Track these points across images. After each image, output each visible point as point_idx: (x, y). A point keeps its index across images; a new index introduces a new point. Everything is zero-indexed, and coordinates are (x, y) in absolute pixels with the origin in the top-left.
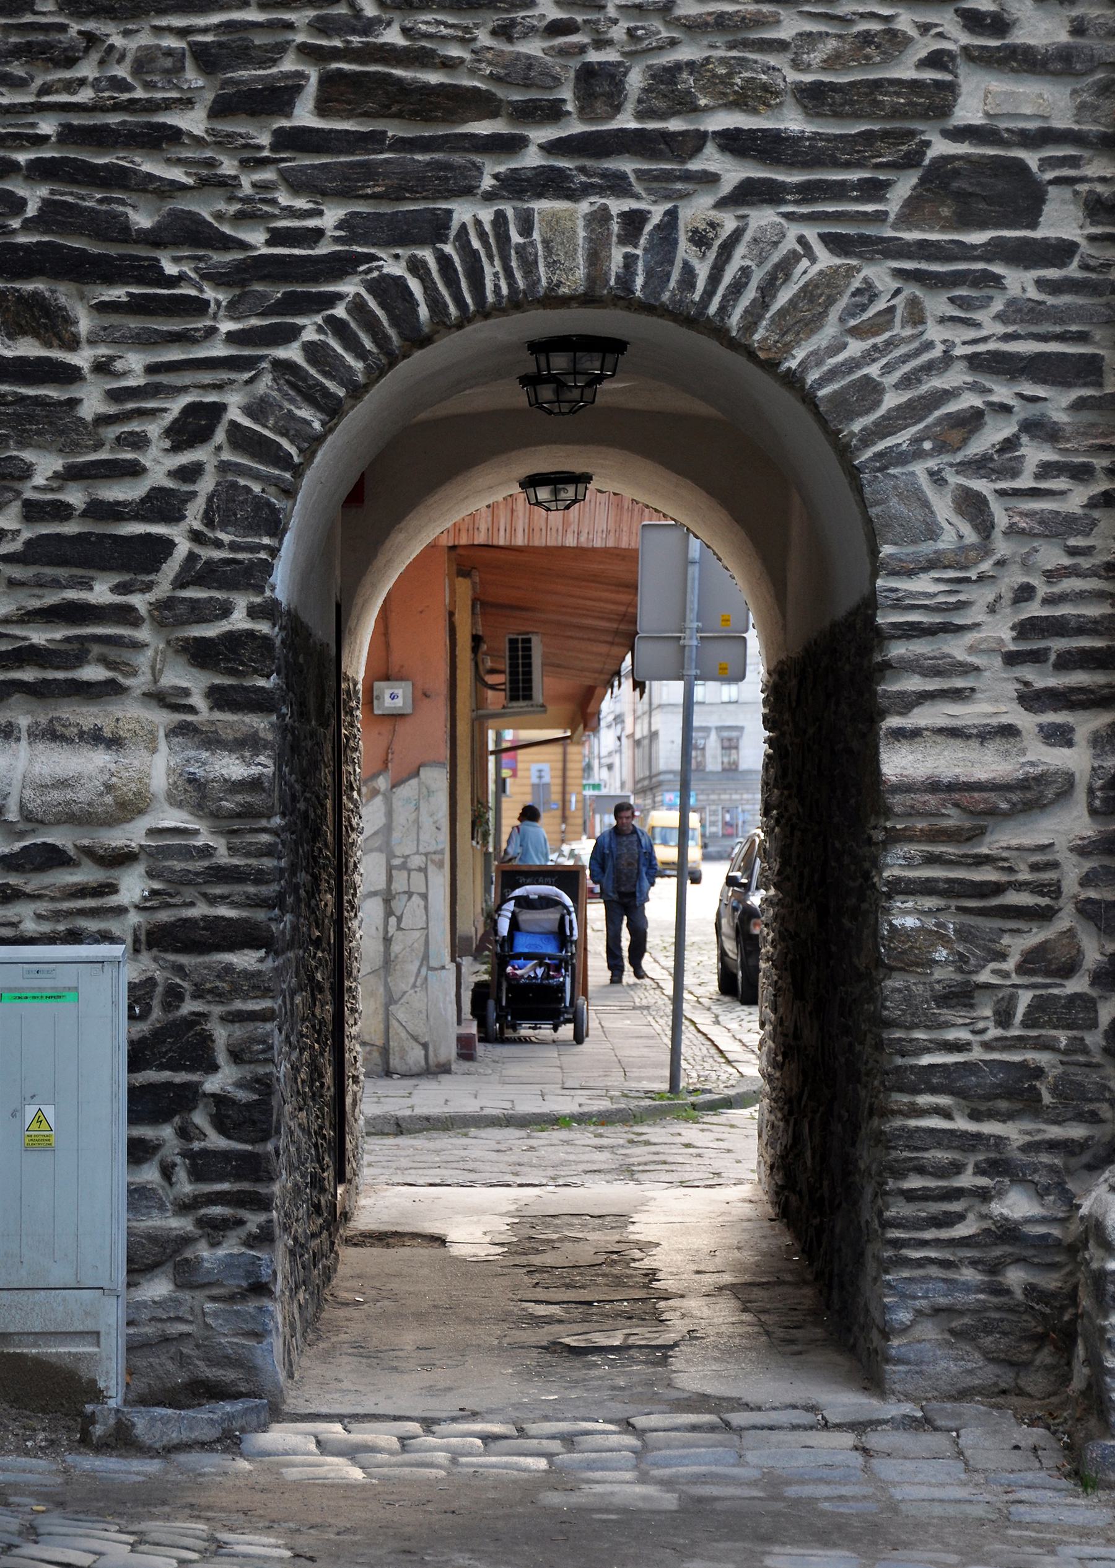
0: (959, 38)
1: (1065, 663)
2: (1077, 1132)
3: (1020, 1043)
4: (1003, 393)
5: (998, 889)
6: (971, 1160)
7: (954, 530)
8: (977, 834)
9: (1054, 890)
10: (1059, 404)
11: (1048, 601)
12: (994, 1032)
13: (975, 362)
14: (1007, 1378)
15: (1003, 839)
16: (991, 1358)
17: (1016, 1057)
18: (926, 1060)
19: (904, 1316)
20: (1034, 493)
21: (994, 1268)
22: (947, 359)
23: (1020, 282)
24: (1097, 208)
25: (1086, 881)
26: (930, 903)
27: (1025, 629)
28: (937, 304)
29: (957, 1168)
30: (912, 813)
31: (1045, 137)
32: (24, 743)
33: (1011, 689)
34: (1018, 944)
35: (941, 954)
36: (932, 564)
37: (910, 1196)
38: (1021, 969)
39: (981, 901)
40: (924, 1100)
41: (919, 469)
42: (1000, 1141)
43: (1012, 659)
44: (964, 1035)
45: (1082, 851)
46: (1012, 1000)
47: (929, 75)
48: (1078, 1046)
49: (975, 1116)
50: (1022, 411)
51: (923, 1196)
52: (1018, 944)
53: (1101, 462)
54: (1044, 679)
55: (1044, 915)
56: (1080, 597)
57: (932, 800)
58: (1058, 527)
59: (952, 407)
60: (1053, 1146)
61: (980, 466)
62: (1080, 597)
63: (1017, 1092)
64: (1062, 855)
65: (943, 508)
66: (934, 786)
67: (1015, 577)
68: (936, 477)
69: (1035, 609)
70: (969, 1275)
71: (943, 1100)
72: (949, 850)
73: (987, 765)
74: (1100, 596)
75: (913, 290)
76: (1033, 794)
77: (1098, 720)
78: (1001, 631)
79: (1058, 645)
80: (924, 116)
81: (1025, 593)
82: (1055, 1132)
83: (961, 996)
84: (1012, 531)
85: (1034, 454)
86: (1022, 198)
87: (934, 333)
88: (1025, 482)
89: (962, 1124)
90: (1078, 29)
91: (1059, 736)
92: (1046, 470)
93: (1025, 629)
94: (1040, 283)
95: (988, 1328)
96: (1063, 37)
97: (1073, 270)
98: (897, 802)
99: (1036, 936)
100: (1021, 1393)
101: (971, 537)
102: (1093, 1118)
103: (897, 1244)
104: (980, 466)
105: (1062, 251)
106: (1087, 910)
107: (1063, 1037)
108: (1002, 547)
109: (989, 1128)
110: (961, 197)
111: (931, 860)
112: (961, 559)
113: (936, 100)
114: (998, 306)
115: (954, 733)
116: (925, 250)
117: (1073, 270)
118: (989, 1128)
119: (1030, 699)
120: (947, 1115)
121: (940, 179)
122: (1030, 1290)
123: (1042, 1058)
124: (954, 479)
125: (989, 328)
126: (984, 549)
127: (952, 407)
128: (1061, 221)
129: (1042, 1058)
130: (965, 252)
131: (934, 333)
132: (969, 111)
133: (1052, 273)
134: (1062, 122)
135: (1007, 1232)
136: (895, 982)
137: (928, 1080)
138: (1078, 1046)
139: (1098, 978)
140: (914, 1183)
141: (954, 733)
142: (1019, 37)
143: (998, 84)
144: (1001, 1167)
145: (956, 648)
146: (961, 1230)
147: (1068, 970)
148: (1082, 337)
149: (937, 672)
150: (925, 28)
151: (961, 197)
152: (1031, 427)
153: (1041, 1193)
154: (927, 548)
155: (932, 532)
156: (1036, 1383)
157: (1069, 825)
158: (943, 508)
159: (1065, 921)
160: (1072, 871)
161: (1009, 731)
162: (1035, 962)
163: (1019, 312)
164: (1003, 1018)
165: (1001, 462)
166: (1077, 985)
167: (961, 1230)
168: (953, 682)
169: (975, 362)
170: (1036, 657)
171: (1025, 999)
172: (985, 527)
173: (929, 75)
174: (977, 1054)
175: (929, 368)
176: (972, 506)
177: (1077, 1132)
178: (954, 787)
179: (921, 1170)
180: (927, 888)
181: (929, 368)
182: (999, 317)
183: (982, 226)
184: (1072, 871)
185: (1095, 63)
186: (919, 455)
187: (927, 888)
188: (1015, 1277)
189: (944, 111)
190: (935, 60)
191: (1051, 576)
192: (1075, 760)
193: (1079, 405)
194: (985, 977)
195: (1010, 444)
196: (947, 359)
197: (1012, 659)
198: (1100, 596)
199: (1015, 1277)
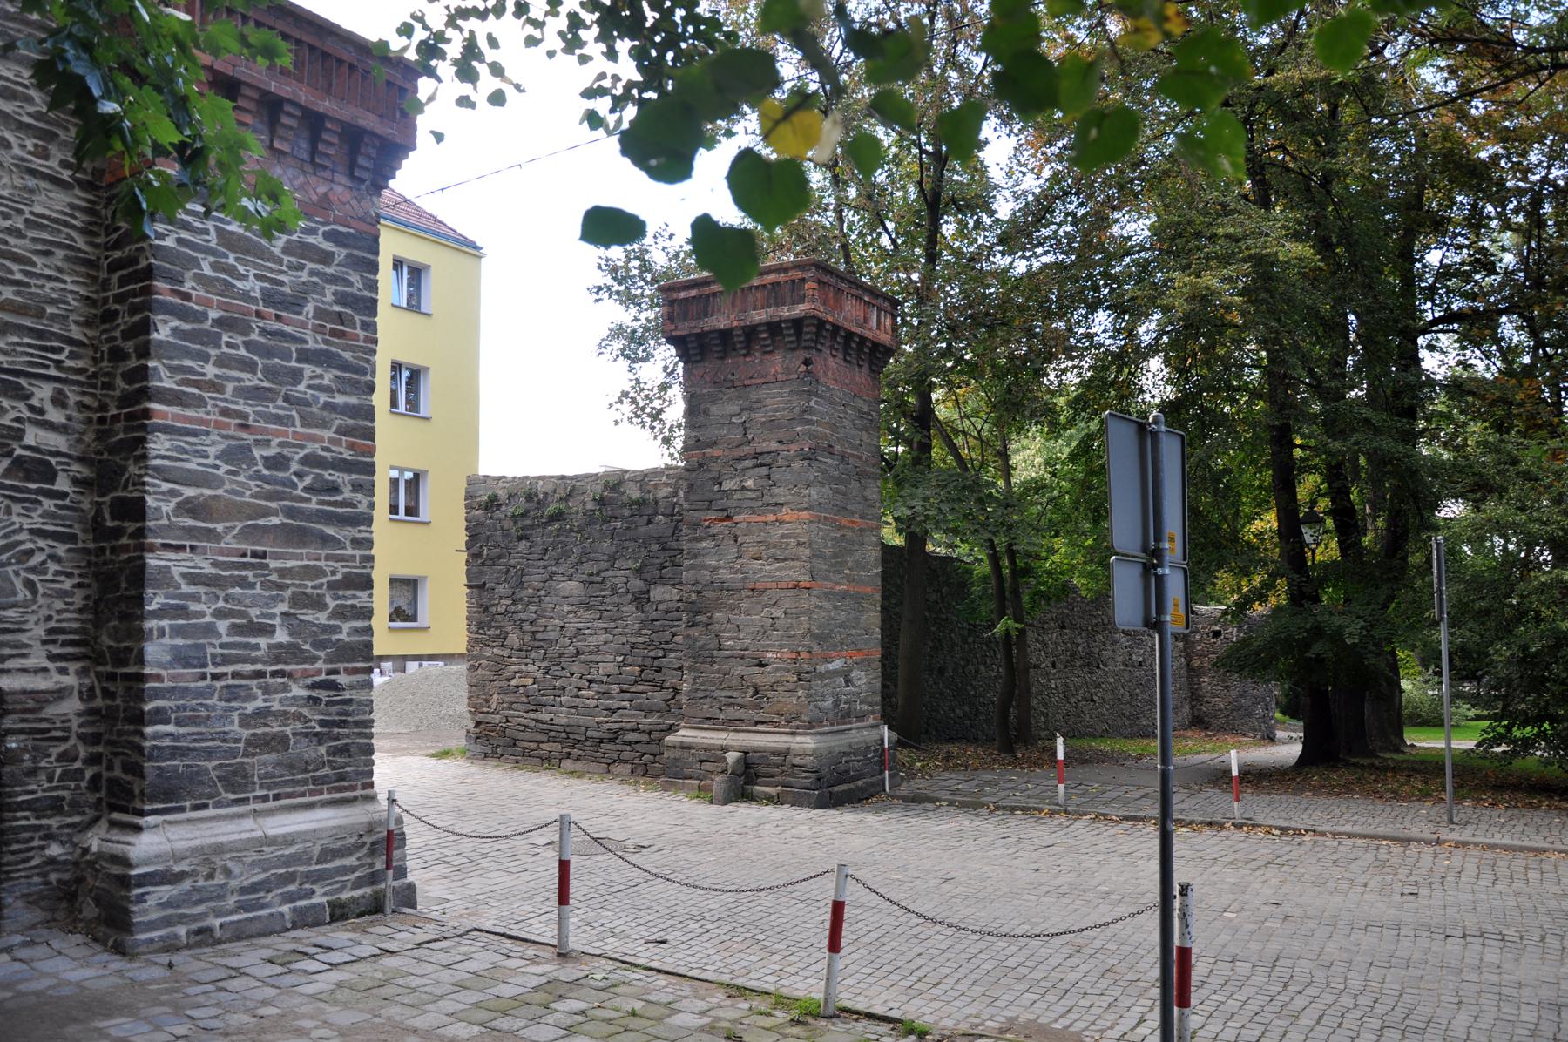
0: (26, 414)
1: (64, 644)
2: (77, 819)
3: (56, 788)
4: (41, 543)
5: (49, 730)
6: (37, 835)
7: (23, 594)
8: (41, 709)
9: (68, 730)
10: (61, 549)
11: (59, 621)
12: (46, 785)
13: (31, 531)
14: (49, 916)
15: (50, 711)
16: (43, 909)
17: (54, 794)
18: (20, 799)
19: (10, 900)
20: (53, 581)
21: (45, 875)
22: (21, 529)
23: (48, 504)
24: (75, 481)
25: (80, 726)
26: (22, 737)
27: (50, 631)
28: (17, 508)
29: (32, 839)
30: (15, 702)
31: (57, 454)
32: (410, 878)
33: (44, 654)
34: (55, 751)
35: (27, 757)
36: (14, 605)
37: (13, 853)
38: (57, 760)
39: (42, 735)
40: (19, 814)
41: (10, 569)
42: (49, 827)
43: (44, 642)
44: (34, 787)
45: (79, 715)
46: (54, 772)
47: (15, 425)
48: (78, 787)
49: (38, 818)
50: (48, 551)
51: (20, 851)
52: (55, 751)
53: (77, 572)
54: (56, 650)
55: (65, 739)
56: (69, 620)
57: (23, 697)
58: (62, 594)
59: (23, 547)
60: (68, 826)
61: (33, 570)
62: (69, 620)
63: (56, 806)
64: (71, 716)
65: (18, 585)
66: (24, 692)
67: (45, 612)
68: (17, 573)
69: (53, 624)
70: (36, 879)
71: (27, 814)
72: (30, 716)
73: (41, 683)
74: (77, 620)
75: (7, 502)
76: (60, 694)
77: (78, 665)
78: (40, 632)
79: (62, 637)
80: (14, 438)
81: (49, 618)
82: (69, 820)
83: (33, 772)
84: (45, 595)
85: (53, 567)
86: (51, 476)
87: (15, 518)
88: (49, 577)
89: (34, 822)
90: (69, 418)
91: (63, 671)
92: (57, 573)
93: (50, 631)
94: (56, 506)
95: (43, 898)
96: (63, 420)
97: (67, 502)
98: (9, 698)
99: (63, 747)
100: (54, 920)
101: (29, 596)
102: (84, 813)
103: (8, 872)
104: (33, 570)
105: (64, 495)
106: (80, 737)
107: (73, 785)
108: (41, 601)
109: (44, 822)
110: (26, 470)
111: (23, 720)
112: (25, 604)
113: (19, 435)
114: (40, 512)
115: (24, 670)
116: (13, 488)
117: (67, 502)
118: (44, 822)
119: (52, 658)
120: (27, 818)
121: (19, 463)
122: (59, 881)
123: (64, 793)
124: (23, 574)
125: (37, 520)
126: (34, 601)
127: (23, 547)
128: (63, 484)
129: (64, 793)
130: (29, 491)
131: (15, 518)
132: (29, 439)
133: (60, 502)
134: (64, 449)
135: (52, 861)
136: (7, 769)
137: (21, 806)
138: (78, 787)
139: (85, 762)
140: (15, 847)
141: (24, 670)
142: (48, 417)
143: (42, 433)
144: (49, 837)
145: (23, 638)
146: (33, 863)
147: (74, 759)
148: (70, 526)
149: (16, 647)
150: (13, 408)
151: (26, 470)
152: (53, 557)
153: (63, 844)
154: (12, 599)
155: (15, 594)
156: (60, 915)
157: (72, 705)
158: (18, 585)
159: (73, 741)
160: (74, 723)
161: (45, 670)
162: (62, 757)
163: (46, 514)
164: (50, 780)
165: (40, 569)
166: (78, 765)
167: (33, 863)
168: (22, 650)
169: (31, 531)
170: (54, 642)
171: (59, 771)
172: (34, 591)
173: (15, 425)
174: (40, 794)
175: (14, 532)
176: (30, 585)
177: (77, 819)
178: (32, 692)
179: (18, 842)
180: (21, 731)
181: (14, 532)
182: (41, 516)
183: (34, 482)
184: (74, 723)
185: (75, 431)
186: (10, 564)
187: (21, 731)
188: (53, 877)
189: (21, 439)
190: (18, 420)
191: (59, 612)
192: (70, 680)
193: (69, 550)
194: (43, 764)
195: (44, 563)
196: (21, 529)
197: (44, 642)
198: (77, 620)
199: (53, 877)
